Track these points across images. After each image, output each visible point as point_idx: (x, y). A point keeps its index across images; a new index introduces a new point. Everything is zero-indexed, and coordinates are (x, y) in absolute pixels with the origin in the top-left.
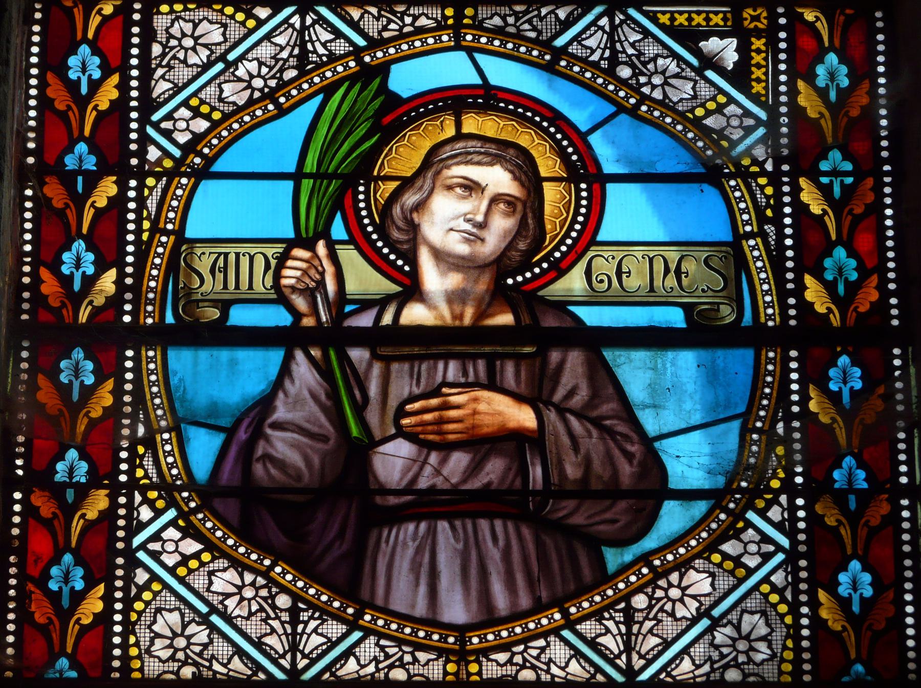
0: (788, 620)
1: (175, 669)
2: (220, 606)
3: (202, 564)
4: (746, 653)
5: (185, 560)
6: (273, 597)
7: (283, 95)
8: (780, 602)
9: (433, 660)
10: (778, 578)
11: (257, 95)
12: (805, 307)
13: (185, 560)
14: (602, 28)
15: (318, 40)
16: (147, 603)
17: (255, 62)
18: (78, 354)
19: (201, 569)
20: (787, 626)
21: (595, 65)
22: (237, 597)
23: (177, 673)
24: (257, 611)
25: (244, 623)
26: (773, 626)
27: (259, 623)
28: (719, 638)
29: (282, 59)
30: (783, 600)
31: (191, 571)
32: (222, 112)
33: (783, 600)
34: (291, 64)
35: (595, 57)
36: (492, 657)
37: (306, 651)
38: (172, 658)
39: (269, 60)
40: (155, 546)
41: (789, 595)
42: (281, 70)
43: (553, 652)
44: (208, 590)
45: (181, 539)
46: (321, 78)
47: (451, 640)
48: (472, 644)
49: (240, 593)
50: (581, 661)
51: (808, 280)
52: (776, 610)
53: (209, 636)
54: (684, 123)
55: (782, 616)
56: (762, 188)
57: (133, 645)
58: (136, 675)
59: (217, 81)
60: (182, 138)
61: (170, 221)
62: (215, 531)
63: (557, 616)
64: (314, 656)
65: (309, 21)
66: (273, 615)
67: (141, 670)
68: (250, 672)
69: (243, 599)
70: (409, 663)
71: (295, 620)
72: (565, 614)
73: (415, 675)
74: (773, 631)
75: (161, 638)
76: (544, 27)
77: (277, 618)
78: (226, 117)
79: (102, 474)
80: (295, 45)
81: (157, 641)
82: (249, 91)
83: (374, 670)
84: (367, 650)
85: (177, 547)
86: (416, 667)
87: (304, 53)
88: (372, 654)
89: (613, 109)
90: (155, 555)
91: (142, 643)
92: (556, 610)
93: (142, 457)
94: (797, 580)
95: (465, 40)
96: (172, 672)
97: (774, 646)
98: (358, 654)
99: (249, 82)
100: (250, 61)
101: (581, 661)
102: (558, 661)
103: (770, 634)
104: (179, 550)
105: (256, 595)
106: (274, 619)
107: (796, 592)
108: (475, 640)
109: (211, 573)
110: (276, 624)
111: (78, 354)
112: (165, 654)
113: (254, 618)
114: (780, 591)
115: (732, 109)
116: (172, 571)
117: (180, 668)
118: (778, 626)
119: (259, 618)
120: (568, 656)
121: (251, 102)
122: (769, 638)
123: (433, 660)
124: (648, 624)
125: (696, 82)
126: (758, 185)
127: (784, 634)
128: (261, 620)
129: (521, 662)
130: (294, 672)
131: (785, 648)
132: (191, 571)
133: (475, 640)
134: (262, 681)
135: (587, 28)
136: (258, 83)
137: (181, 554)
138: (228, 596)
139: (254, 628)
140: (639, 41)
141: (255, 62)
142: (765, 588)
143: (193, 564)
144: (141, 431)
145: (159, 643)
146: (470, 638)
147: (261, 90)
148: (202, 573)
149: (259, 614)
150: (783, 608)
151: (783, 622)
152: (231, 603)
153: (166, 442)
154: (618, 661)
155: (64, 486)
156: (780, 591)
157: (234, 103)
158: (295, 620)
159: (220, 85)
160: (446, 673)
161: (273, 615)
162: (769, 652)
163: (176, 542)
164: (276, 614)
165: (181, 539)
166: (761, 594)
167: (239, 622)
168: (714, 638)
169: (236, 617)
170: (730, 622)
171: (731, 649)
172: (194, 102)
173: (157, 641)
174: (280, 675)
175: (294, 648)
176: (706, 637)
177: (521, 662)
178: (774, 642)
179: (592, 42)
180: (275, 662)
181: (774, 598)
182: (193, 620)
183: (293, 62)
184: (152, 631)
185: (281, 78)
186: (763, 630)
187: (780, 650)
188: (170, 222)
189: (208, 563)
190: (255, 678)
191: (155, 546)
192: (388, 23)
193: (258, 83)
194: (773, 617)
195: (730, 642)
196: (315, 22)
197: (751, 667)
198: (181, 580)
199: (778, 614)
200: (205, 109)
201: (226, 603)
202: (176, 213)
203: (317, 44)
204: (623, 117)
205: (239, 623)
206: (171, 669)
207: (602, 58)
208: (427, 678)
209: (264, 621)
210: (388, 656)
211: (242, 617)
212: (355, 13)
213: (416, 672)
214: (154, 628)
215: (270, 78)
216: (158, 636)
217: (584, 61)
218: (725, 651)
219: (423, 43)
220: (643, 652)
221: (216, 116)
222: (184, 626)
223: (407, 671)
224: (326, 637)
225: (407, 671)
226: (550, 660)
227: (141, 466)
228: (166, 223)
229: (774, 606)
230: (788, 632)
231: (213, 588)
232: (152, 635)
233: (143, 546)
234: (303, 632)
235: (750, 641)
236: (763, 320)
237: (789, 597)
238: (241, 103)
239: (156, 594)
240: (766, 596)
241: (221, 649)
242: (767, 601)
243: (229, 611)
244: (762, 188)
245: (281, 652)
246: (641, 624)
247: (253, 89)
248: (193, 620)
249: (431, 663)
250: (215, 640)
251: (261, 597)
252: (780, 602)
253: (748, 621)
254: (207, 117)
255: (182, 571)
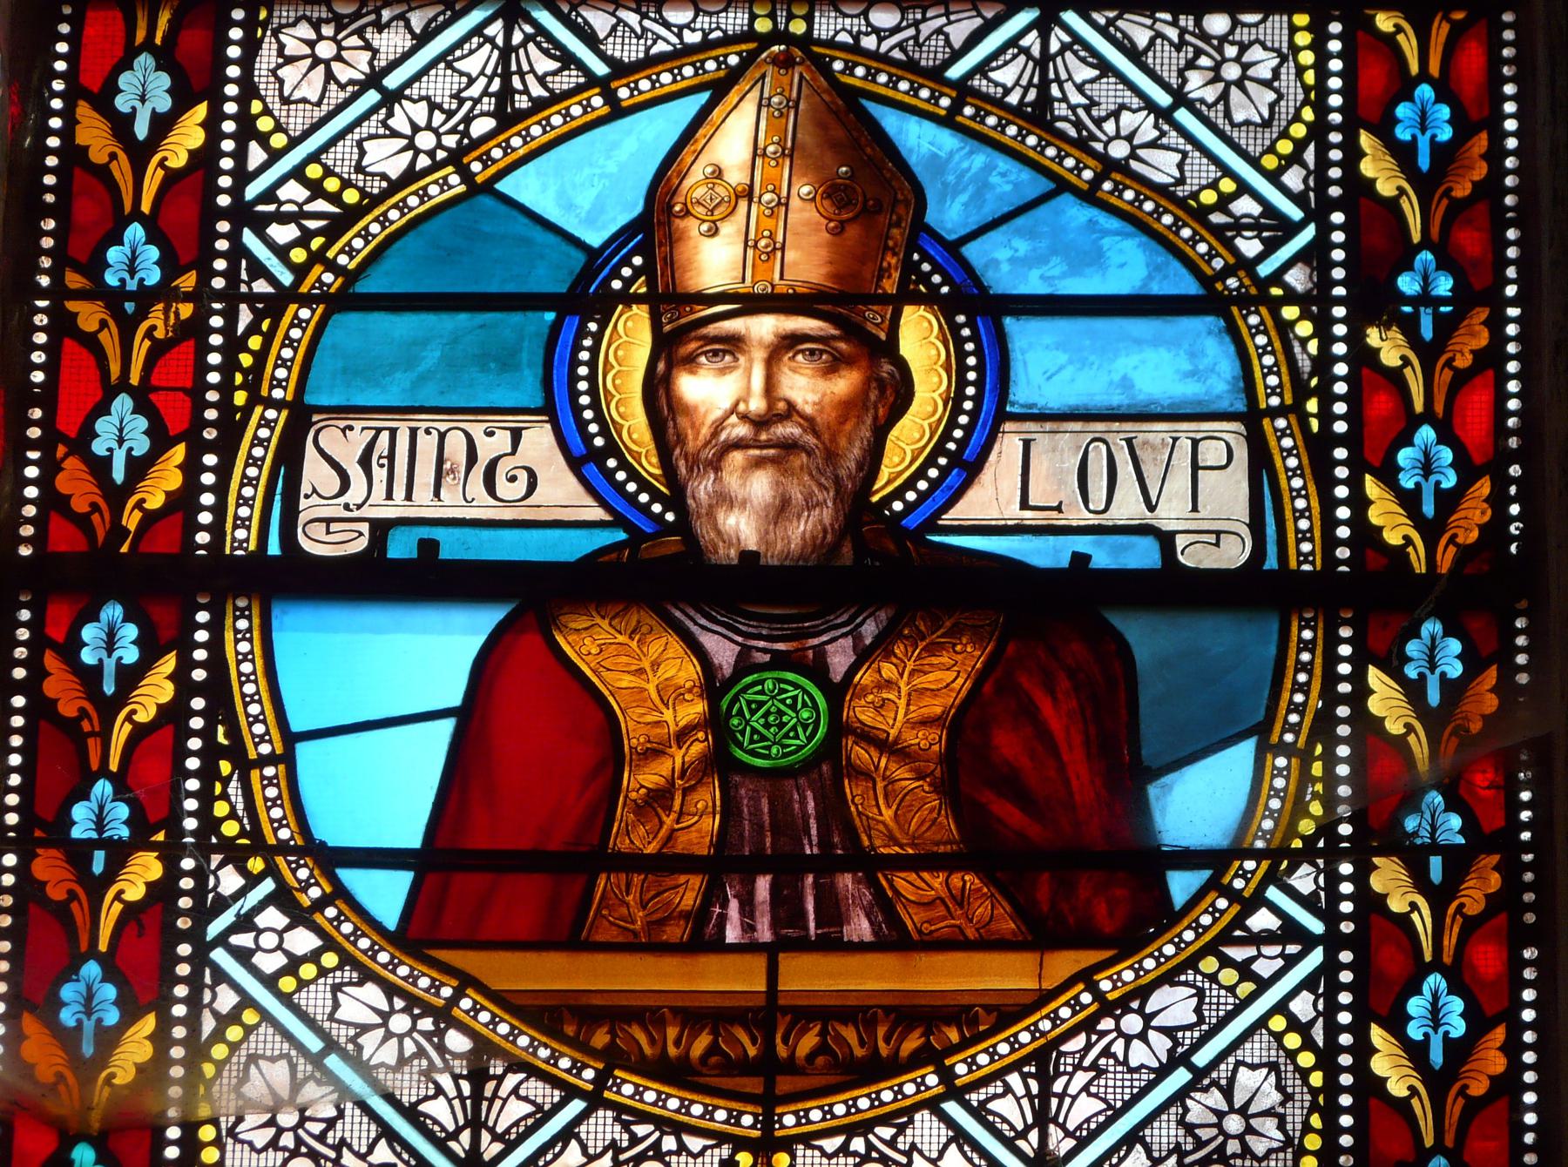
0: (1317, 1079)
1: (1238, 30)
2: (350, 1047)
3: (323, 972)
4: (1240, 1137)
5: (293, 964)
6: (440, 1033)
7: (1084, 1007)
8: (1302, 1048)
9: (712, 1147)
10: (1303, 1006)
11: (423, 162)
12: (1365, 534)
13: (293, 964)
14: (1026, 51)
15: (532, 71)
16: (1284, 134)
17: (424, 104)
18: (113, 612)
19: (1195, 188)
20: (1314, 1092)
21: (515, 1065)
22: (381, 1032)
23: (1236, 23)
24: (1106, 119)
25: (390, 1076)
26: (272, 79)
27: (1103, 100)
28: (1196, 1114)
29: (1086, 1070)
30: (1308, 1044)
31: (1214, 185)
32: (362, 191)
33: (1308, 1044)
34: (485, 108)
35: (512, 1080)
36: (817, 1143)
37: (499, 1129)
38: (1244, 48)
39: (447, 99)
40: (243, 940)
41: (1318, 1034)
42: (468, 120)
43: (918, 1132)
44: (1185, 154)
45: (288, 928)
46: (1016, 1040)
47: (747, 1120)
48: (783, 1127)
49: (385, 1024)
50: (966, 1148)
51: (1374, 676)
52: (1294, 1062)
53: (1185, 81)
54: (1168, 216)
55: (1304, 1074)
56: (233, 815)
57: (1306, 68)
58: (1302, 20)
59: (1205, 1027)
60: (1262, 920)
61: (1279, 772)
62: (1192, 238)
63: (932, 1080)
64: (513, 1137)
65: (517, 38)
66: (1081, 112)
67: (1293, 30)
68: (1120, 23)
69: (389, 1035)
70: (670, 1153)
71: (478, 1076)
72: (947, 1075)
73: (857, 16)
74: (274, 72)
75: (1269, 68)
76: (609, 1129)
77: (1073, 108)
78: (1192, 963)
79: (153, 821)
80: (494, 74)
81: (1268, 75)
82: (1148, 1010)
83: (922, 27)
84: (600, 1129)
85: (281, 940)
86: (855, 29)
87: (506, 93)
88: (609, 1136)
89: (1045, 185)
90: (243, 956)
91: (1293, 71)
92: (931, 1069)
93: (226, 782)
94: (1333, 1008)
95: (756, 1116)
96: (1244, 25)
97: (1290, 1127)
98: (583, 1136)
99: (411, 139)
100: (415, 101)
101: (966, 1148)
102: (925, 1148)
103: (279, 66)
104: (285, 946)
105: (414, 1028)
106: (1079, 106)
107: (1332, 1030)
108: (789, 1120)
109: (336, 988)
110: (1076, 98)
111: (113, 612)
112: (1256, 53)
113: (1112, 107)
114: (1303, 1029)
115: (270, 963)
116: (270, 982)
117: (1232, 31)
118: (263, 80)
119: (1103, 106)
120: (943, 1140)
121: (1144, 993)
122: (280, 60)
123: (712, 1147)
124: (475, 91)
125: (331, 1018)
126: (240, 820)
127: (1307, 1104)
128: (1099, 104)
129: (862, 1150)
130: (1043, 26)
131: (1307, 1128)
132: (302, 984)
133: (789, 1120)
134: (1099, 10)
135: (522, 1138)
136: (425, 140)
137: (287, 953)
138: (365, 1028)
139: (1108, 94)
140: (1092, 81)
141: (424, 104)
142: (1278, 1023)
143: (308, 971)
144: (1312, 406)
145: (1264, 72)
146: (781, 1115)
147: (431, 154)
148: (321, 988)
149: (1103, 113)
150: (1306, 1059)
151: (1305, 1082)
152: (1148, 133)
153: (1271, 386)
154: (1021, 1143)
155: (89, 846)
156: (1303, 1029)
157: (384, 176)
158: (478, 1076)
159: (360, 144)
160: (809, 19)
161: (1081, 112)
162: (1279, 1136)
163: (280, 934)
164: (1075, 113)
165: (288, 928)
166: (1271, 1033)
167: (1136, 102)
168: (1186, 1110)
169: (1140, 109)
170: (342, 87)
171: (1215, 1131)
172: (314, 171)
173: (1268, 75)
174: (1070, 17)
175: (476, 1124)
176: (1173, 1110)
177: (862, 1150)
178: (274, 53)
179: (1005, 76)
180: (1077, 38)
181: (1292, 1041)
182: (1209, 107)
183: (488, 104)
184: (1277, 91)
185: (466, 133)
186: (290, 74)
187: (1298, 1134)
188: (1280, 770)
189: (333, 970)
190: (1111, 14)
191: (243, 940)
192: (894, 1138)
193: (425, 140)
194: (270, 93)
195: (1214, 1120)
196: (528, 38)
197: (316, 15)
198: (286, 999)
199: (1298, 1069)
200: (332, 185)
201: (1156, 133)
202: (1271, 787)
203: (530, 79)
204: (1067, 199)
205: (381, 1076)
206: (1246, 30)
207: (500, 1079)
208: (837, 10)
209: (1093, 103)
210: (635, 1140)
211: (1130, 109)
212: (600, 21)
213: (856, 21)
214: (1272, 96)
215: (1110, 1032)
216: (1267, 84)
217: (533, 1071)
218: (1205, 1134)
219: (831, 1112)
220: (488, 47)
221: (1209, 964)
222: (1224, 97)
223: (868, 24)
224: (533, 1103)
225: (868, 24)
226: (913, 1146)
227: (225, 796)
228: (1288, 768)
229: (1292, 1055)
230: (1314, 1102)
231: (339, 1015)
232: (1276, 84)
233: (222, 940)
234: (495, 1095)
235: (313, 55)
236: (1293, 564)
237: (1319, 1039)
238: (394, 175)
239: (1271, 150)
240: (1278, 1037)
241: (1166, 60)
242: (1281, 1046)
243: (365, 1056)
244: (233, 815)
245: (1068, 55)
246: (485, 93)
247: (417, 152)
248: (1209, 107)
249: (709, 1152)
250: (1174, 74)
251: (422, 1033)
252: (1302, 1048)
253: (1247, 1080)
254: (335, 198)
255: (287, 984)
